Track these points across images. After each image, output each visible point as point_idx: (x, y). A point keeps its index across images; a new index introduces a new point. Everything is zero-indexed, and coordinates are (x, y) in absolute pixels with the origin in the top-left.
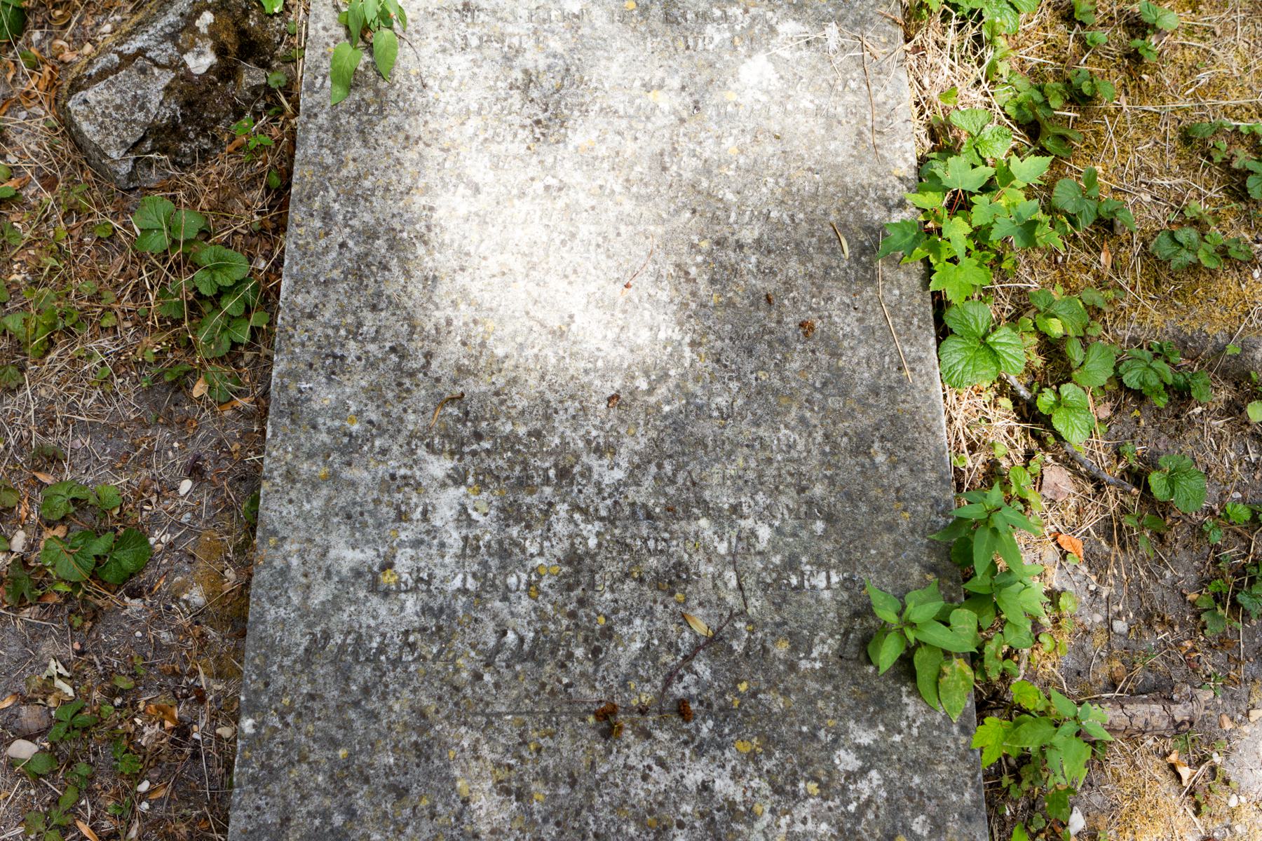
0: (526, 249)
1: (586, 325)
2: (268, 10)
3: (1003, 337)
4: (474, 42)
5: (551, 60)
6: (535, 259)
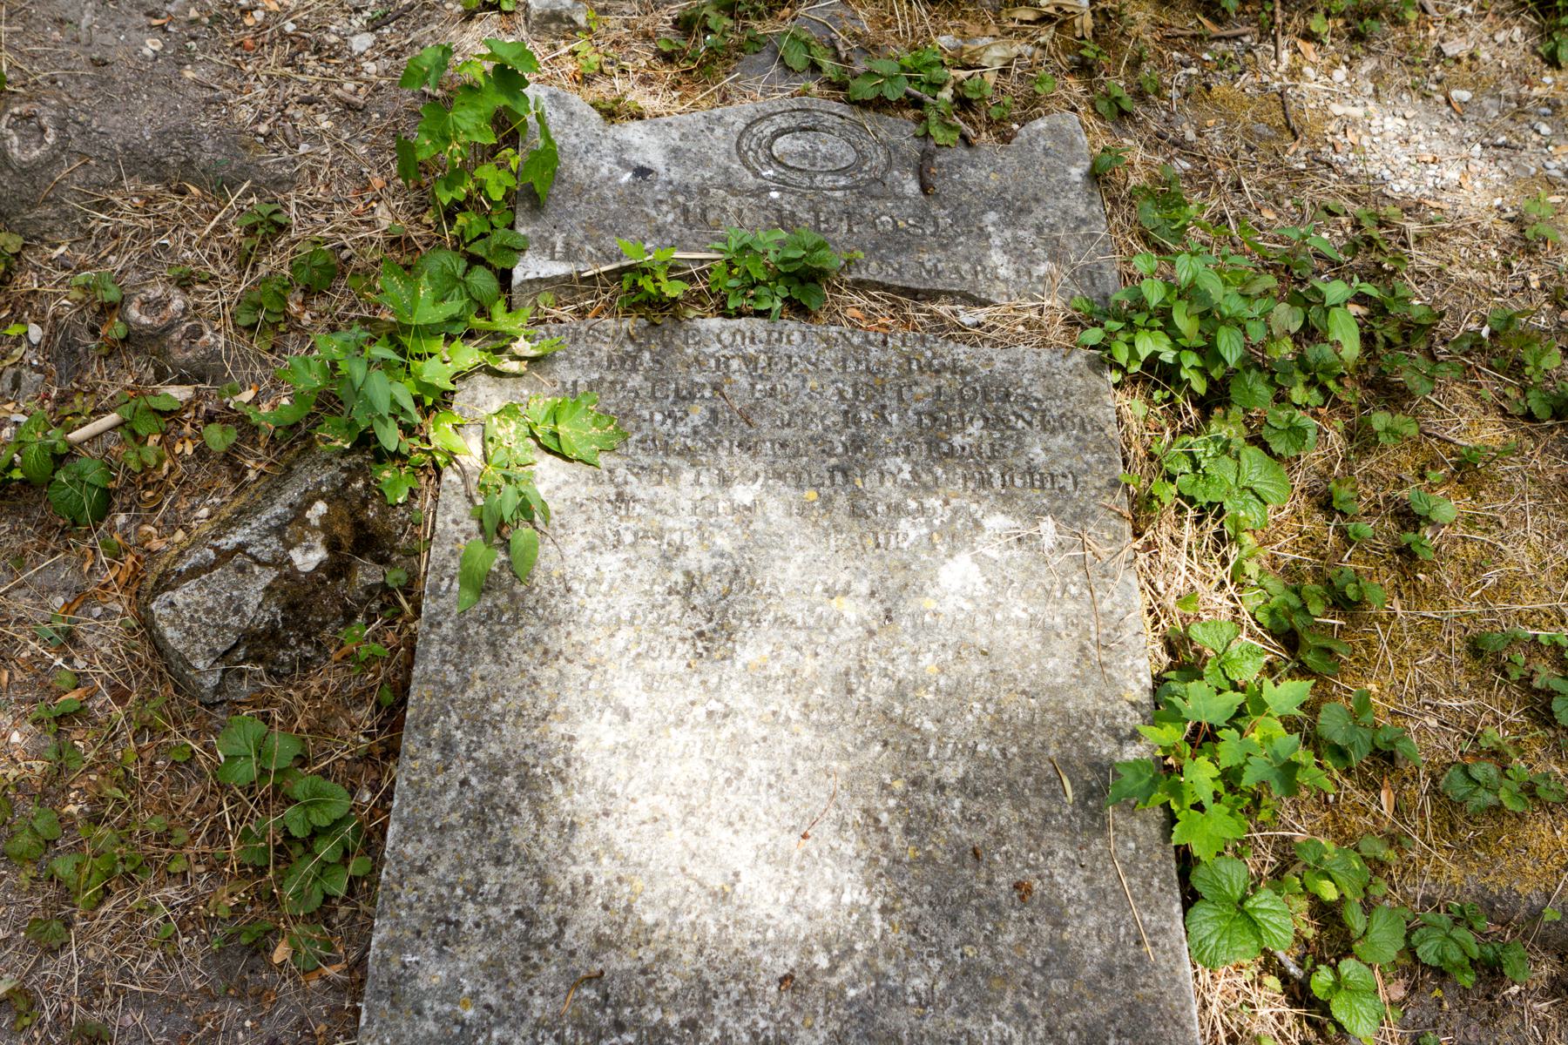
0: (682, 790)
1: (754, 885)
2: (390, 500)
3: (1264, 901)
4: (628, 538)
5: (717, 560)
6: (694, 802)
